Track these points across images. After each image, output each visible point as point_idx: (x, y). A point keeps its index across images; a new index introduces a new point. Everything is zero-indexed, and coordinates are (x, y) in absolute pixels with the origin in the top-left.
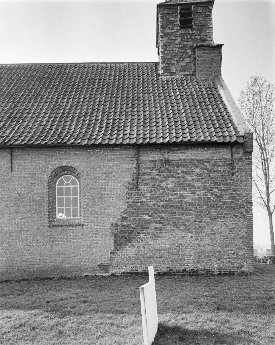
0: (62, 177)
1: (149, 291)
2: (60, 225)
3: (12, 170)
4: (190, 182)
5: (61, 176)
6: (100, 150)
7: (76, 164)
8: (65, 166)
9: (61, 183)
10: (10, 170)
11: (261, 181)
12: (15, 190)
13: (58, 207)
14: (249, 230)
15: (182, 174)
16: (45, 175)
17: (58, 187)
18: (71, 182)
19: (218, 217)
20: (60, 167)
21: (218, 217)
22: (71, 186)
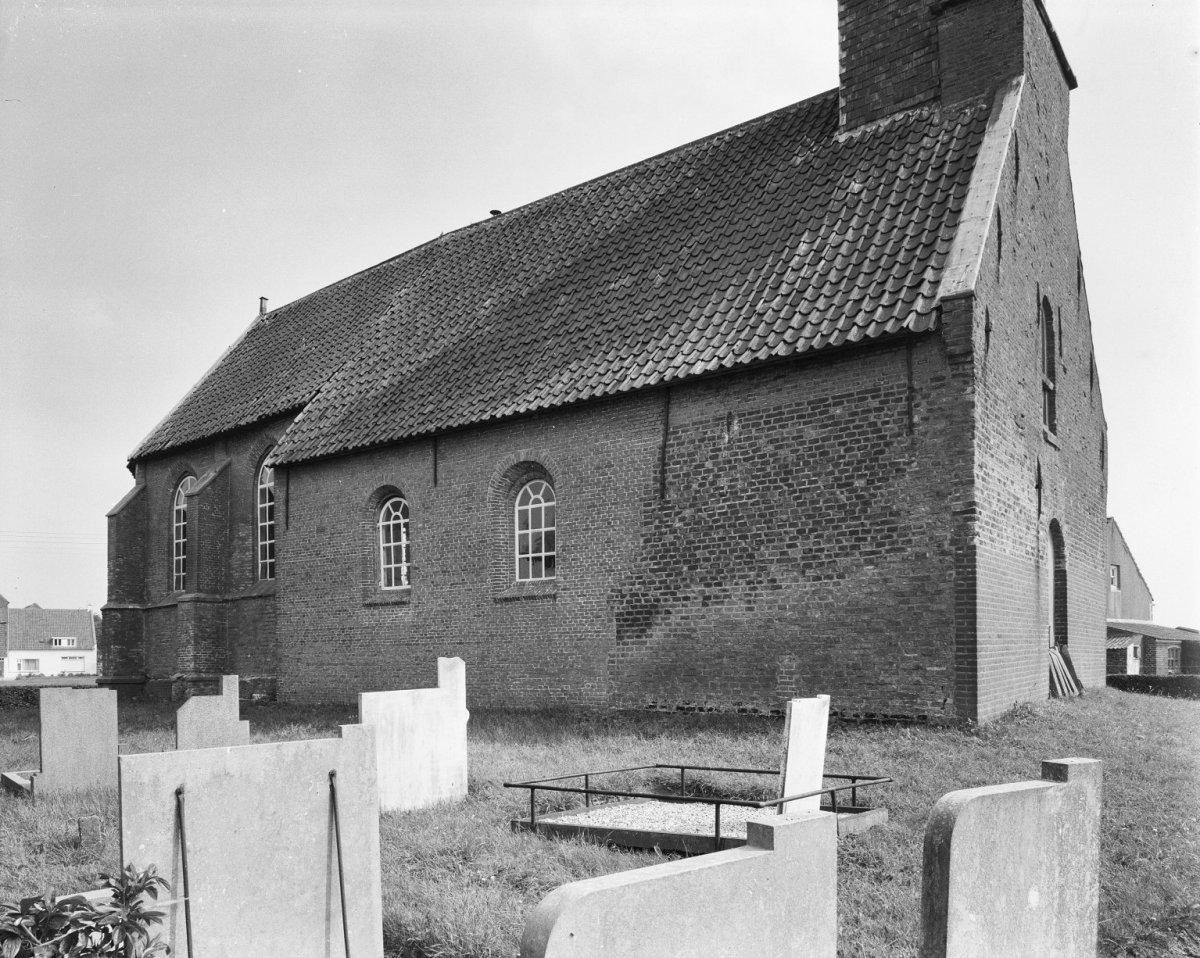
0: (527, 487)
1: (810, 715)
2: (912, 373)
3: (436, 482)
4: (820, 443)
5: (524, 485)
6: (353, 474)
7: (544, 454)
8: (524, 462)
9: (525, 500)
10: (431, 484)
11: (1036, 76)
12: (441, 525)
13: (520, 554)
14: (962, 573)
15: (771, 447)
16: (490, 488)
17: (519, 511)
18: (543, 496)
19: (865, 560)
20: (517, 465)
21: (865, 560)
22: (543, 505)
